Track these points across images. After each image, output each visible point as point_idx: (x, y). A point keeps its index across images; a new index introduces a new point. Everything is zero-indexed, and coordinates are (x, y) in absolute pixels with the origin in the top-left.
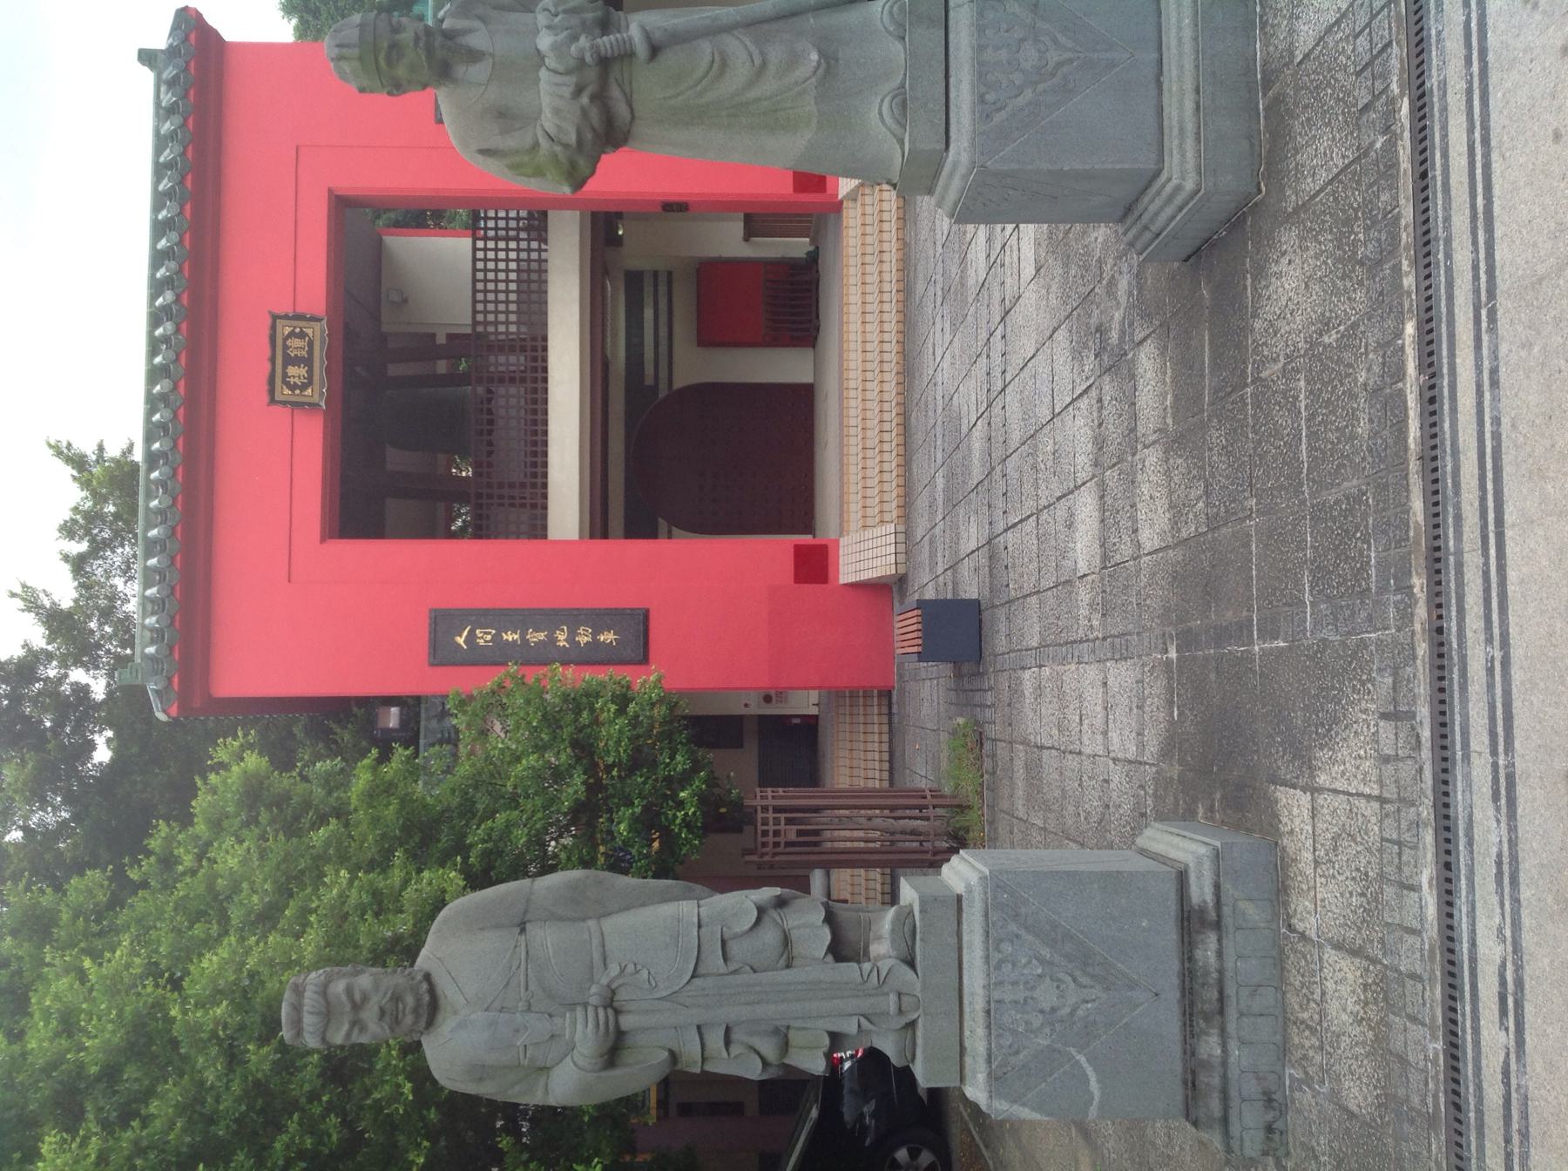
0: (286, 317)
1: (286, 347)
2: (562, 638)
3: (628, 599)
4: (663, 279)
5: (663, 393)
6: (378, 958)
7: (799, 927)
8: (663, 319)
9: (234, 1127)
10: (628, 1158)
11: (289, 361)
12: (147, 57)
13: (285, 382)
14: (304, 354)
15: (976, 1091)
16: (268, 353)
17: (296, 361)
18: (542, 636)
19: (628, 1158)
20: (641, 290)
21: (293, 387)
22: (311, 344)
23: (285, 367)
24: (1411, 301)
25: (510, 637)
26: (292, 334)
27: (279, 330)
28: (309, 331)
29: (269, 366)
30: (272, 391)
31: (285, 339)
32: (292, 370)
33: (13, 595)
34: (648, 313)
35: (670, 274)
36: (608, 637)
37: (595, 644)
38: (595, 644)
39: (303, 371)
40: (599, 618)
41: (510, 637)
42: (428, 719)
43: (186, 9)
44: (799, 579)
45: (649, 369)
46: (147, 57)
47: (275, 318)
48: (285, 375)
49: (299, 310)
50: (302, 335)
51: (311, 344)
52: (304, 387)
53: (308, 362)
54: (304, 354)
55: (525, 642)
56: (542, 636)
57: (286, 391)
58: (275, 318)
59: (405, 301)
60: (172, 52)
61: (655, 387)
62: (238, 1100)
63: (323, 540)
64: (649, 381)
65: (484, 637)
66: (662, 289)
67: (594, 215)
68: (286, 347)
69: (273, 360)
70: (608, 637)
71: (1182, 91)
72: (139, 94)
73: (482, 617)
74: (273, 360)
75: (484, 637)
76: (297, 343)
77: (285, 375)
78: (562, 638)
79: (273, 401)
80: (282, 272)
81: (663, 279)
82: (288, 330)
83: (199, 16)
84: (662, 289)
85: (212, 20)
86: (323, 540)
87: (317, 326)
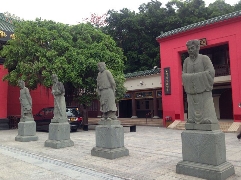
0: (206, 40)
2: (167, 84)
3: (172, 92)
15: (51, 124)
18: (167, 81)
22: (203, 44)
24: (87, 168)
25: (167, 77)
26: (204, 41)
33: (238, 1)
36: (167, 90)
37: (167, 88)
38: (167, 88)
40: (170, 89)
41: (167, 77)
44: (176, 115)
49: (207, 42)
50: (204, 43)
51: (203, 44)
55: (166, 79)
56: (167, 81)
58: (206, 39)
63: (178, 52)
65: (167, 74)
67: (231, 82)
70: (167, 90)
71: (192, 164)
73: (169, 73)
75: (167, 74)
78: (167, 84)
82: (204, 41)
87: (206, 44)
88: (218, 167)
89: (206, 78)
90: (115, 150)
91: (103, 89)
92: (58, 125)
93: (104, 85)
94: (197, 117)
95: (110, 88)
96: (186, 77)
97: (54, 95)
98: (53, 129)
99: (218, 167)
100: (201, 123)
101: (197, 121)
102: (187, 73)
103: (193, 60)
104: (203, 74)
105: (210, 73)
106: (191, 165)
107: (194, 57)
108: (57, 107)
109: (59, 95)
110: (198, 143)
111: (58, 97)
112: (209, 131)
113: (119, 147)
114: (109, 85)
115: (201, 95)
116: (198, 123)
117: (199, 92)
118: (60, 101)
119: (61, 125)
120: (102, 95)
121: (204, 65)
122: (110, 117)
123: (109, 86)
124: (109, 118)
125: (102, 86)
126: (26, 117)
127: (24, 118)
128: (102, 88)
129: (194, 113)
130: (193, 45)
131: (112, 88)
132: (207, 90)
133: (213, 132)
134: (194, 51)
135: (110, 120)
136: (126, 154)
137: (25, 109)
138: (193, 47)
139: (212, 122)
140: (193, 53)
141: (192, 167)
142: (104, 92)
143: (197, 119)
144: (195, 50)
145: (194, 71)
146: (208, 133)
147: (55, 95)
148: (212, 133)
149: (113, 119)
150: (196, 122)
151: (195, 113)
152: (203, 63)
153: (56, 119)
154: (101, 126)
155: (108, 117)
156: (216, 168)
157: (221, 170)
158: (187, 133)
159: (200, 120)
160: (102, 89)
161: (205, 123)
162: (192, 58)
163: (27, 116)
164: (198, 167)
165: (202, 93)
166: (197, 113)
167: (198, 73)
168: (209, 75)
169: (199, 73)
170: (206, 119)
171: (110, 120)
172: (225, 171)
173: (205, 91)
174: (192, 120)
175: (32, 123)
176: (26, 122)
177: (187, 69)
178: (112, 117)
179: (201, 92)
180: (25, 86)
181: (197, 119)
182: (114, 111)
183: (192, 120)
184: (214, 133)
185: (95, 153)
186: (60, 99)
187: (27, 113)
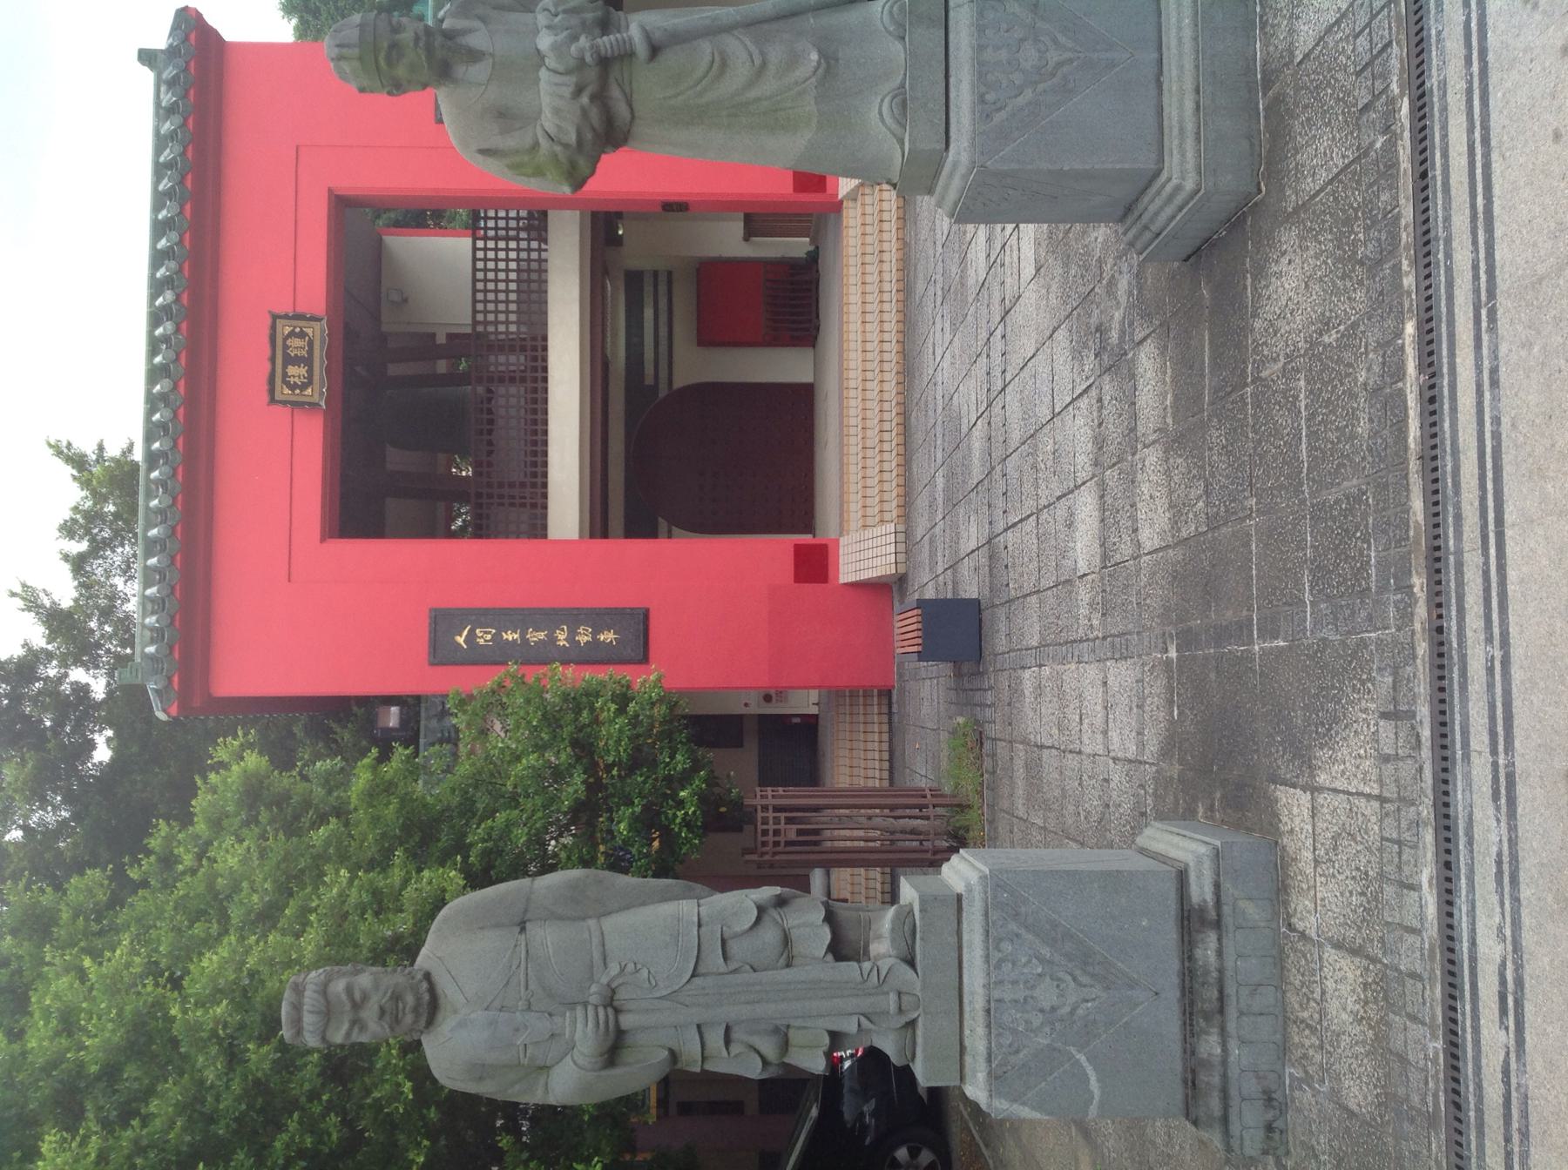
0: (286, 317)
1: (286, 347)
2: (562, 637)
3: (628, 598)
4: (663, 279)
5: (663, 392)
7: (799, 926)
8: (663, 318)
10: (628, 1157)
11: (289, 360)
12: (147, 57)
13: (285, 382)
14: (304, 353)
15: (976, 1090)
16: (268, 353)
17: (296, 361)
18: (542, 635)
19: (628, 1157)
20: (641, 289)
21: (293, 387)
22: (311, 344)
23: (285, 367)
25: (510, 636)
26: (292, 334)
27: (279, 329)
28: (309, 331)
29: (269, 366)
30: (272, 391)
31: (285, 339)
32: (292, 370)
34: (648, 313)
35: (670, 273)
36: (608, 636)
37: (595, 643)
38: (595, 643)
39: (303, 371)
40: (599, 618)
41: (510, 636)
42: (428, 718)
43: (186, 9)
44: (799, 578)
45: (649, 369)
46: (147, 57)
47: (275, 317)
48: (285, 375)
49: (299, 310)
50: (302, 335)
51: (311, 344)
52: (304, 387)
53: (308, 361)
54: (304, 353)
55: (525, 641)
56: (542, 635)
57: (286, 391)
58: (275, 317)
59: (405, 300)
60: (172, 52)
61: (655, 387)
63: (323, 540)
64: (649, 381)
65: (484, 637)
66: (662, 288)
68: (286, 347)
69: (273, 360)
70: (608, 636)
72: (139, 94)
73: (482, 616)
74: (273, 360)
75: (484, 637)
76: (297, 342)
77: (285, 375)
78: (562, 637)
79: (273, 400)
80: (282, 271)
81: (663, 279)
82: (288, 330)
83: (199, 16)
84: (662, 288)
85: (212, 20)
86: (323, 540)
87: (317, 325)
89: (809, 1024)
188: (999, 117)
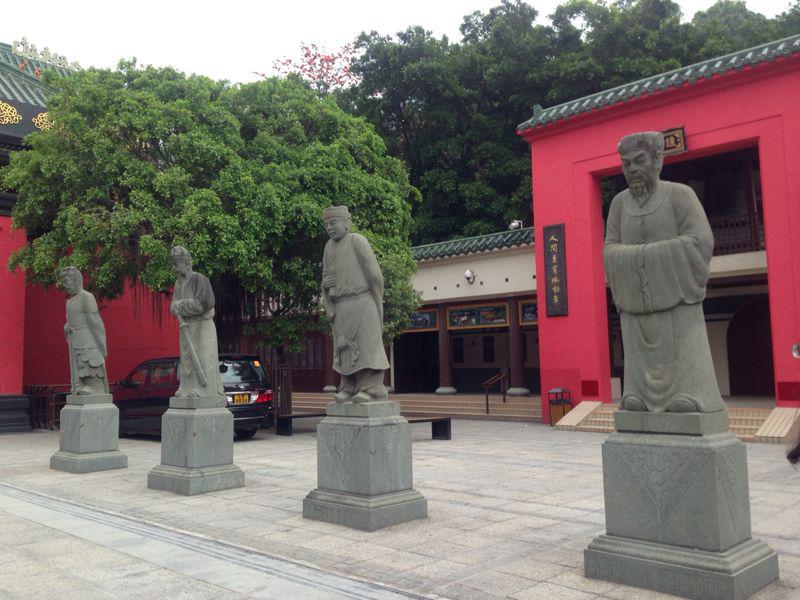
0: (684, 133)
2: (555, 280)
3: (572, 307)
6: (201, 199)
9: (69, 555)
10: (370, 97)
12: (534, 277)
15: (169, 412)
18: (555, 271)
19: (370, 97)
22: (674, 147)
25: (554, 258)
26: (676, 138)
36: (556, 299)
37: (553, 294)
38: (553, 294)
40: (563, 295)
41: (554, 258)
44: (583, 382)
49: (688, 139)
50: (677, 143)
51: (674, 147)
55: (553, 265)
56: (555, 271)
58: (683, 128)
62: (547, 76)
63: (590, 173)
65: (554, 247)
70: (556, 299)
71: (636, 548)
73: (562, 245)
75: (554, 247)
78: (555, 280)
82: (677, 135)
87: (683, 148)
88: (724, 557)
89: (685, 259)
90: (382, 500)
91: (343, 296)
92: (192, 417)
93: (347, 282)
94: (654, 390)
95: (363, 292)
96: (619, 258)
97: (179, 317)
98: (177, 431)
99: (724, 557)
100: (668, 411)
101: (655, 403)
102: (619, 242)
103: (642, 200)
104: (673, 248)
105: (696, 245)
106: (633, 551)
107: (645, 190)
108: (190, 357)
109: (197, 316)
110: (656, 477)
111: (194, 325)
112: (693, 438)
113: (394, 492)
114: (362, 283)
115: (668, 316)
116: (657, 410)
117: (660, 308)
118: (198, 338)
119: (203, 418)
120: (338, 316)
121: (676, 216)
122: (365, 391)
123: (360, 285)
124: (361, 395)
125: (338, 287)
126: (86, 389)
127: (78, 394)
128: (340, 294)
129: (643, 376)
130: (642, 152)
131: (373, 294)
132: (687, 302)
133: (707, 442)
134: (643, 169)
135: (367, 401)
136: (417, 512)
137: (82, 364)
138: (642, 155)
139: (702, 405)
140: (640, 177)
141: (638, 556)
142: (344, 306)
143: (654, 396)
144: (647, 167)
145: (644, 236)
146: (689, 444)
147: (184, 317)
148: (704, 445)
149: (374, 397)
150: (649, 407)
151: (648, 376)
152: (675, 212)
153: (184, 395)
154: (335, 420)
155: (358, 391)
156: (718, 562)
157: (732, 567)
158: (620, 444)
159: (664, 401)
160: (339, 298)
161: (680, 409)
162: (636, 195)
163: (91, 385)
164: (659, 555)
165: (671, 309)
166: (655, 377)
167: (656, 244)
168: (695, 251)
169: (661, 242)
170: (683, 397)
171: (367, 401)
172: (746, 568)
173: (682, 303)
174: (637, 400)
175: (107, 411)
176: (86, 407)
177: (622, 229)
178: (371, 391)
179: (667, 306)
180: (82, 288)
181: (654, 396)
182: (378, 372)
183: (637, 400)
184: (712, 445)
185: (316, 509)
186: (199, 329)
187: (90, 377)
188: (230, 507)
